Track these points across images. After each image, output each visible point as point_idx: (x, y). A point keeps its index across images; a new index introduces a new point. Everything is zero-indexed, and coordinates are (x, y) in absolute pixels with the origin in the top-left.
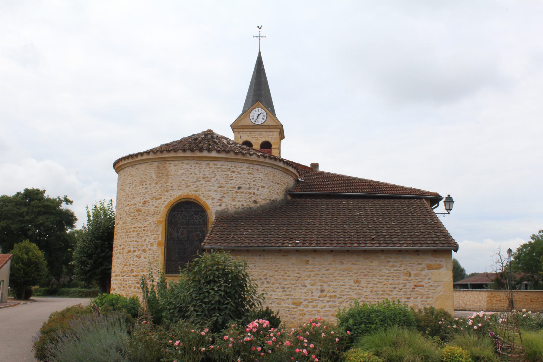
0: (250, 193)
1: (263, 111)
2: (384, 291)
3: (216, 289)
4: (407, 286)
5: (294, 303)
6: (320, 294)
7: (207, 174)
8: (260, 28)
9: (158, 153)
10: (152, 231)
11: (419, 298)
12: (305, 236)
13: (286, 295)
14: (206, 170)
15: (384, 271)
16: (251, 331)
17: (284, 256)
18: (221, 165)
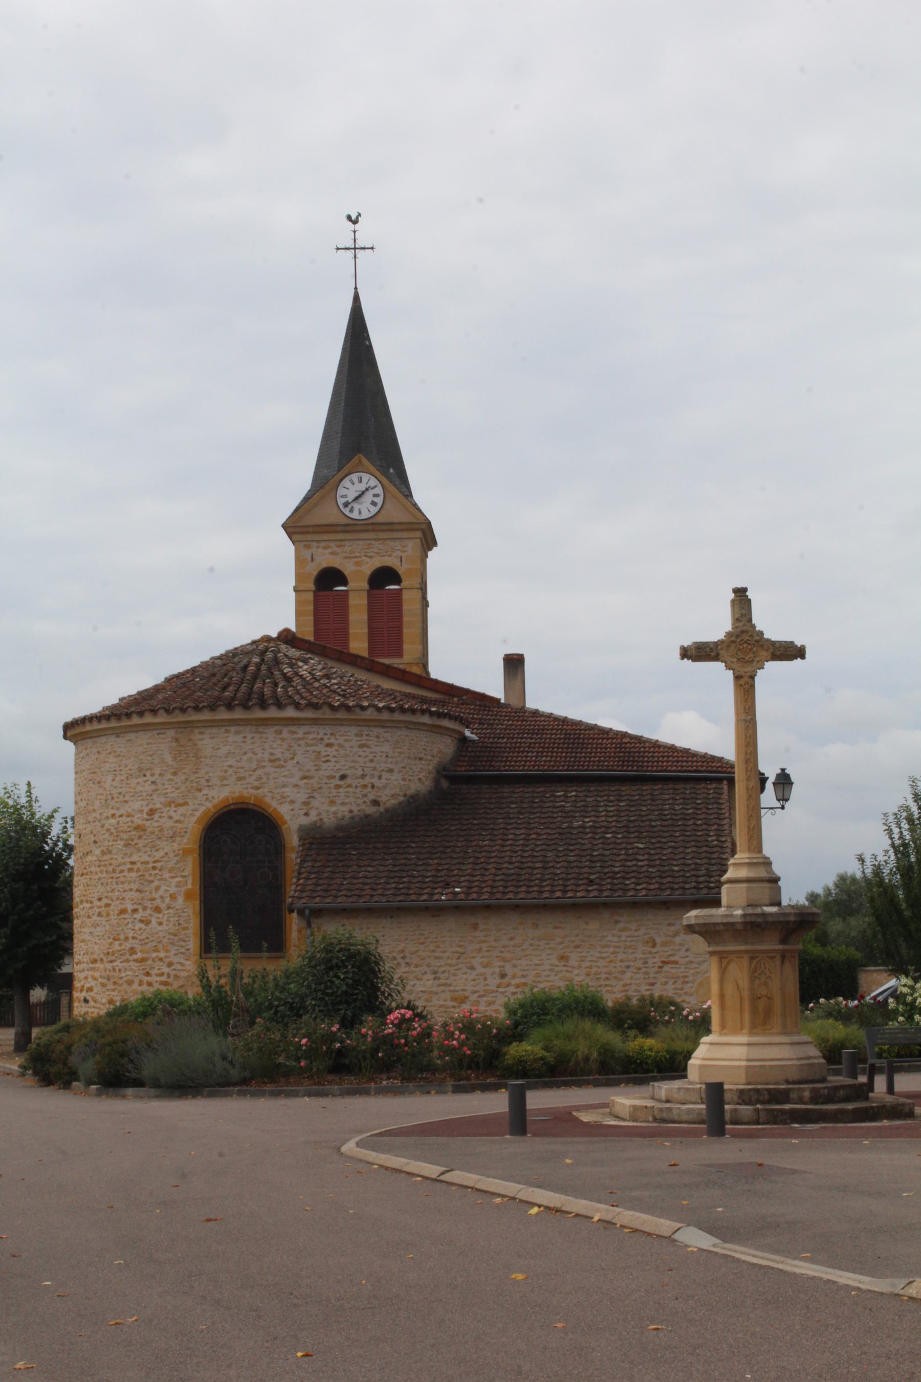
0: (365, 786)
1: (373, 482)
2: (610, 973)
3: (342, 977)
4: (650, 964)
5: (454, 999)
6: (498, 981)
7: (278, 753)
8: (355, 222)
9: (124, 718)
10: (170, 871)
11: (671, 982)
12: (471, 878)
13: (440, 985)
14: (275, 745)
15: (609, 938)
16: (392, 1023)
17: (434, 916)
18: (305, 734)
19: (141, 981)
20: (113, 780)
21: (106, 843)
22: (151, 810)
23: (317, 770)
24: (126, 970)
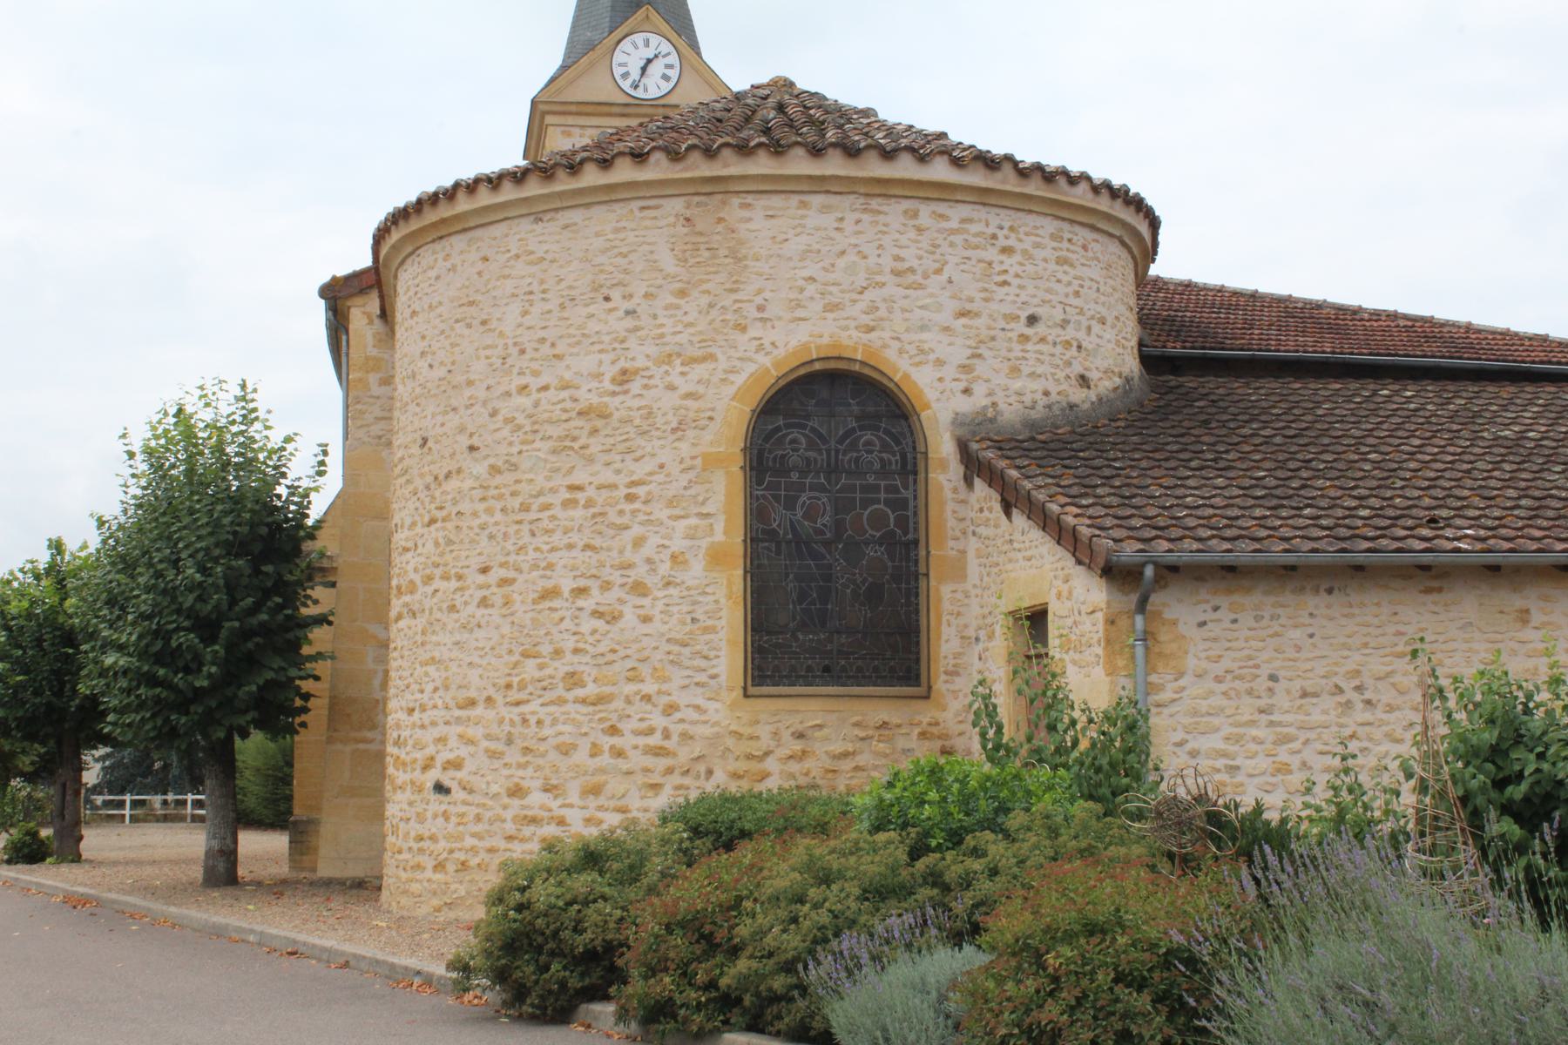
0: (1067, 344)
1: (666, 47)
9: (561, 174)
10: (670, 504)
17: (1428, 591)
18: (963, 221)
19: (594, 745)
20: (525, 313)
21: (503, 449)
22: (624, 372)
23: (986, 300)
24: (555, 722)
